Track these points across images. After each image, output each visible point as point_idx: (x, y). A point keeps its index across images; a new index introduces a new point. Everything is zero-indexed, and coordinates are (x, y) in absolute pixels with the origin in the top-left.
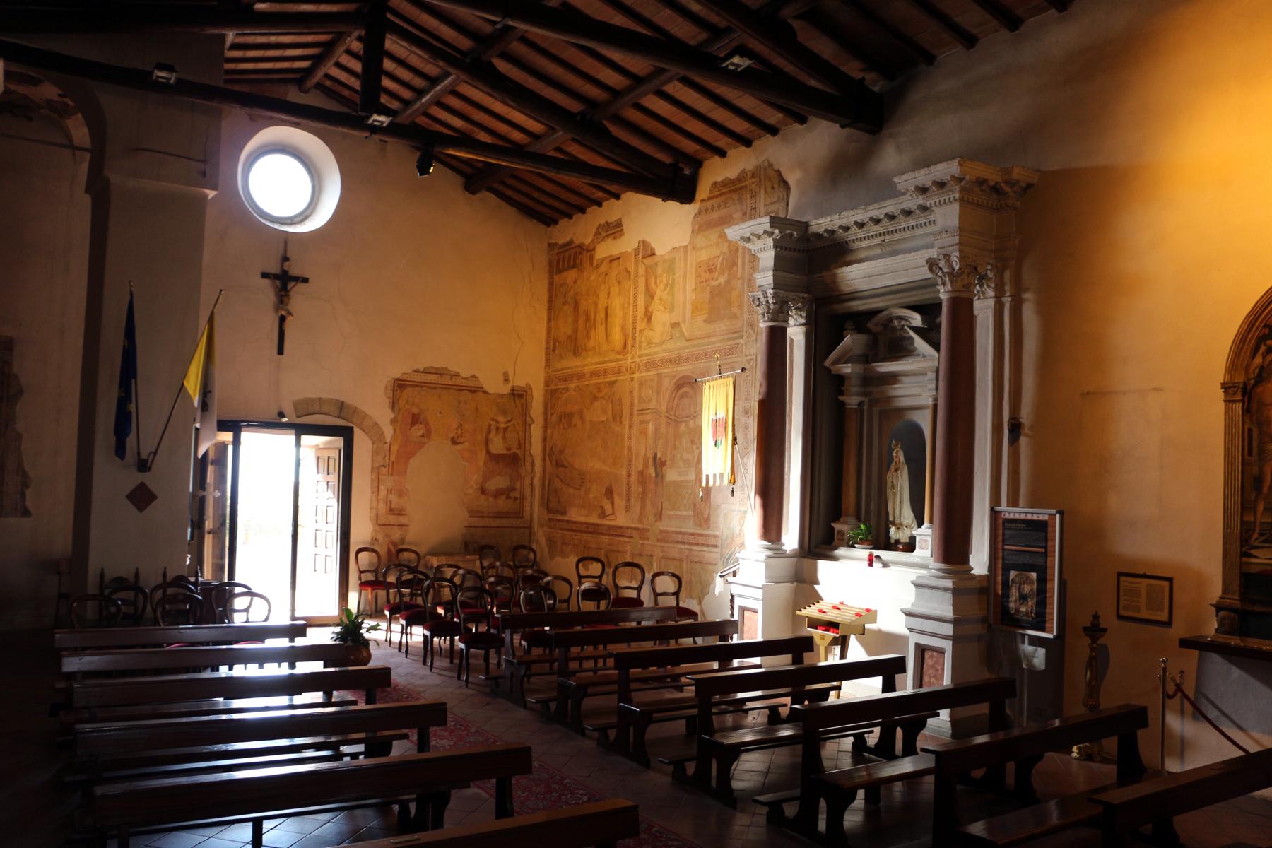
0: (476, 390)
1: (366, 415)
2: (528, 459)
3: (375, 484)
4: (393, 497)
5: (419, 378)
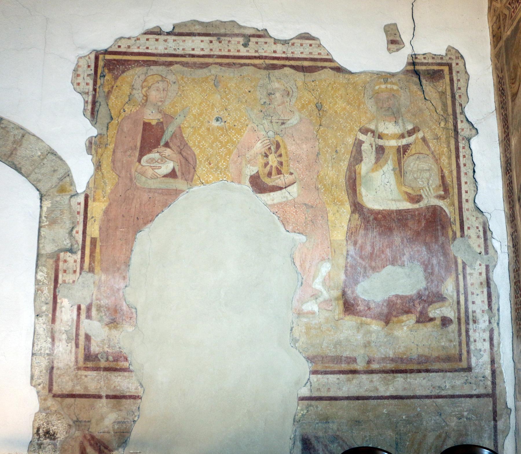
0: (314, 65)
1: (25, 133)
2: (472, 221)
3: (47, 292)
4: (95, 327)
5: (159, 46)
